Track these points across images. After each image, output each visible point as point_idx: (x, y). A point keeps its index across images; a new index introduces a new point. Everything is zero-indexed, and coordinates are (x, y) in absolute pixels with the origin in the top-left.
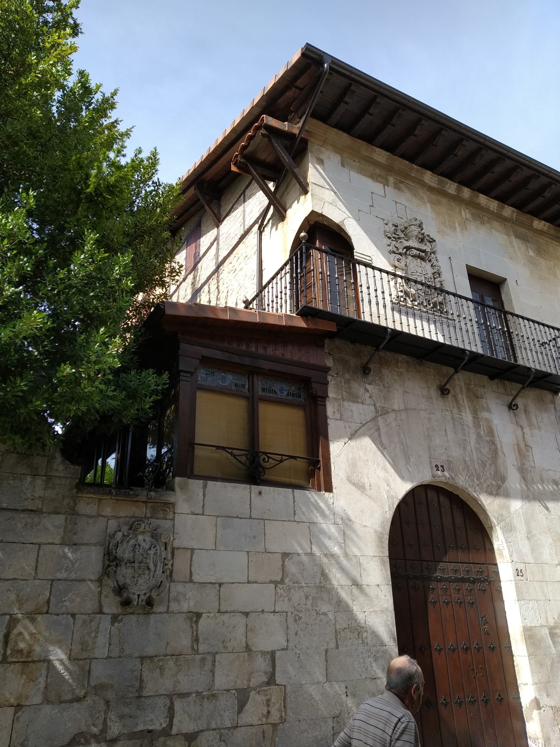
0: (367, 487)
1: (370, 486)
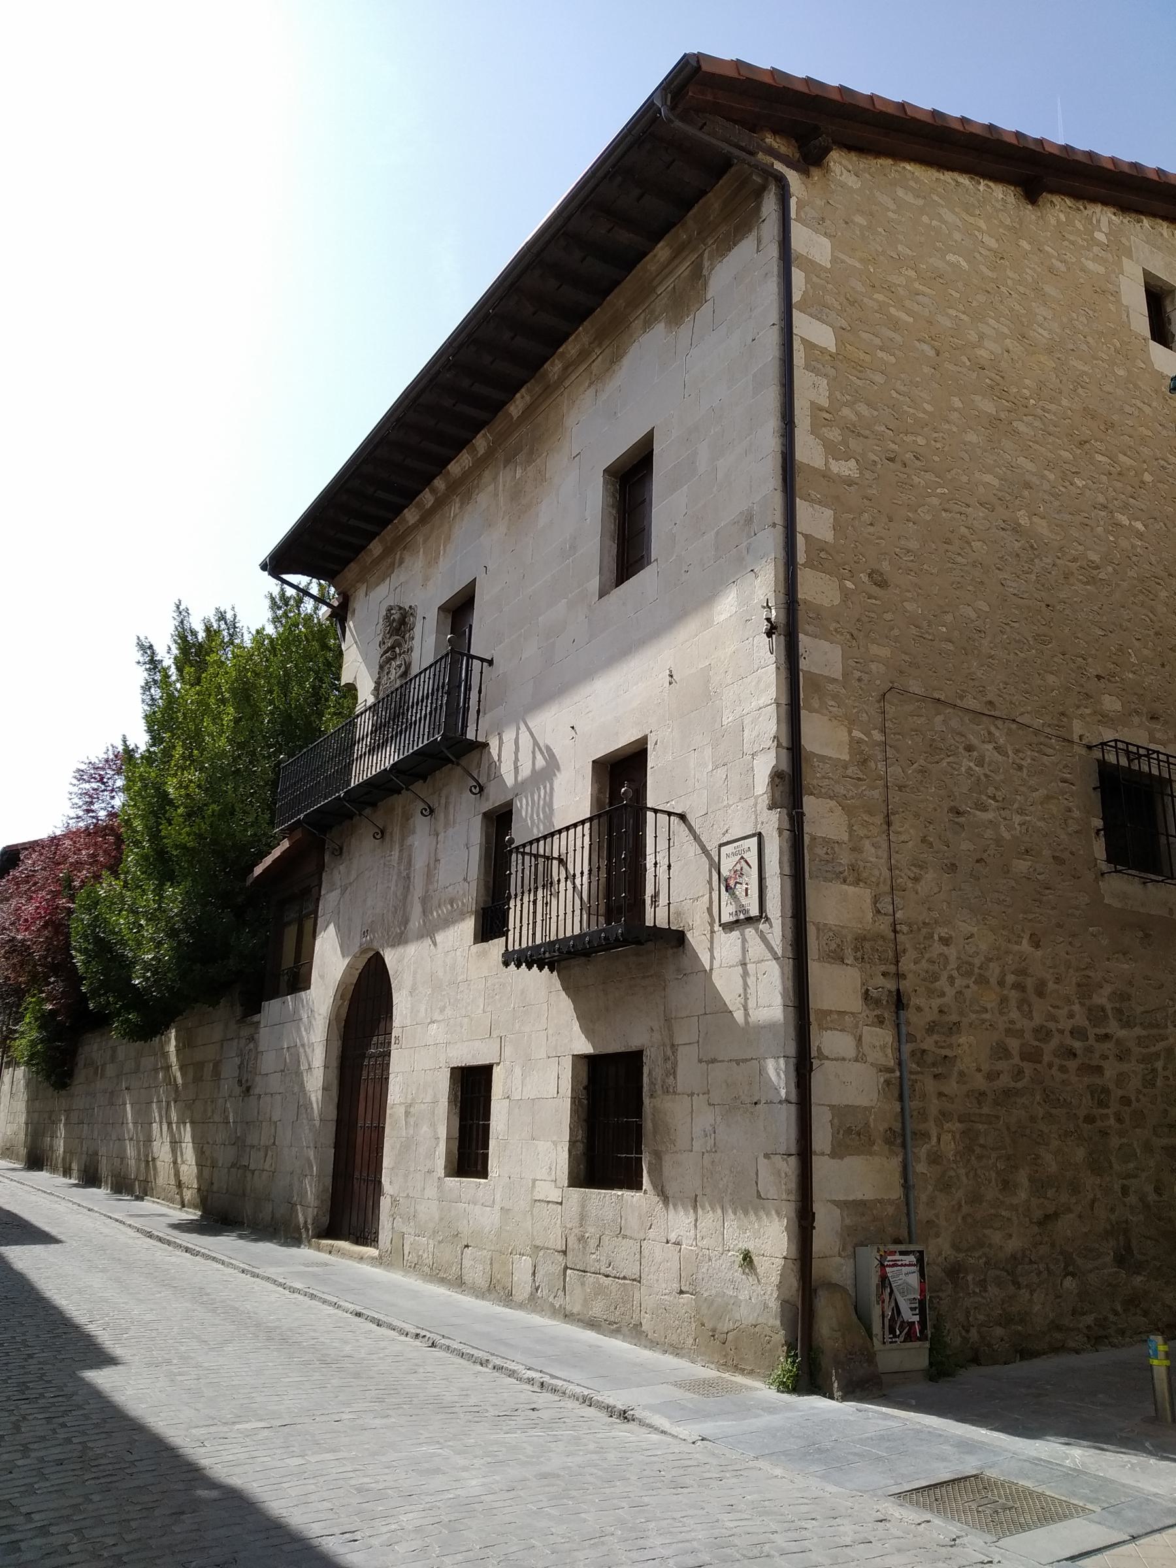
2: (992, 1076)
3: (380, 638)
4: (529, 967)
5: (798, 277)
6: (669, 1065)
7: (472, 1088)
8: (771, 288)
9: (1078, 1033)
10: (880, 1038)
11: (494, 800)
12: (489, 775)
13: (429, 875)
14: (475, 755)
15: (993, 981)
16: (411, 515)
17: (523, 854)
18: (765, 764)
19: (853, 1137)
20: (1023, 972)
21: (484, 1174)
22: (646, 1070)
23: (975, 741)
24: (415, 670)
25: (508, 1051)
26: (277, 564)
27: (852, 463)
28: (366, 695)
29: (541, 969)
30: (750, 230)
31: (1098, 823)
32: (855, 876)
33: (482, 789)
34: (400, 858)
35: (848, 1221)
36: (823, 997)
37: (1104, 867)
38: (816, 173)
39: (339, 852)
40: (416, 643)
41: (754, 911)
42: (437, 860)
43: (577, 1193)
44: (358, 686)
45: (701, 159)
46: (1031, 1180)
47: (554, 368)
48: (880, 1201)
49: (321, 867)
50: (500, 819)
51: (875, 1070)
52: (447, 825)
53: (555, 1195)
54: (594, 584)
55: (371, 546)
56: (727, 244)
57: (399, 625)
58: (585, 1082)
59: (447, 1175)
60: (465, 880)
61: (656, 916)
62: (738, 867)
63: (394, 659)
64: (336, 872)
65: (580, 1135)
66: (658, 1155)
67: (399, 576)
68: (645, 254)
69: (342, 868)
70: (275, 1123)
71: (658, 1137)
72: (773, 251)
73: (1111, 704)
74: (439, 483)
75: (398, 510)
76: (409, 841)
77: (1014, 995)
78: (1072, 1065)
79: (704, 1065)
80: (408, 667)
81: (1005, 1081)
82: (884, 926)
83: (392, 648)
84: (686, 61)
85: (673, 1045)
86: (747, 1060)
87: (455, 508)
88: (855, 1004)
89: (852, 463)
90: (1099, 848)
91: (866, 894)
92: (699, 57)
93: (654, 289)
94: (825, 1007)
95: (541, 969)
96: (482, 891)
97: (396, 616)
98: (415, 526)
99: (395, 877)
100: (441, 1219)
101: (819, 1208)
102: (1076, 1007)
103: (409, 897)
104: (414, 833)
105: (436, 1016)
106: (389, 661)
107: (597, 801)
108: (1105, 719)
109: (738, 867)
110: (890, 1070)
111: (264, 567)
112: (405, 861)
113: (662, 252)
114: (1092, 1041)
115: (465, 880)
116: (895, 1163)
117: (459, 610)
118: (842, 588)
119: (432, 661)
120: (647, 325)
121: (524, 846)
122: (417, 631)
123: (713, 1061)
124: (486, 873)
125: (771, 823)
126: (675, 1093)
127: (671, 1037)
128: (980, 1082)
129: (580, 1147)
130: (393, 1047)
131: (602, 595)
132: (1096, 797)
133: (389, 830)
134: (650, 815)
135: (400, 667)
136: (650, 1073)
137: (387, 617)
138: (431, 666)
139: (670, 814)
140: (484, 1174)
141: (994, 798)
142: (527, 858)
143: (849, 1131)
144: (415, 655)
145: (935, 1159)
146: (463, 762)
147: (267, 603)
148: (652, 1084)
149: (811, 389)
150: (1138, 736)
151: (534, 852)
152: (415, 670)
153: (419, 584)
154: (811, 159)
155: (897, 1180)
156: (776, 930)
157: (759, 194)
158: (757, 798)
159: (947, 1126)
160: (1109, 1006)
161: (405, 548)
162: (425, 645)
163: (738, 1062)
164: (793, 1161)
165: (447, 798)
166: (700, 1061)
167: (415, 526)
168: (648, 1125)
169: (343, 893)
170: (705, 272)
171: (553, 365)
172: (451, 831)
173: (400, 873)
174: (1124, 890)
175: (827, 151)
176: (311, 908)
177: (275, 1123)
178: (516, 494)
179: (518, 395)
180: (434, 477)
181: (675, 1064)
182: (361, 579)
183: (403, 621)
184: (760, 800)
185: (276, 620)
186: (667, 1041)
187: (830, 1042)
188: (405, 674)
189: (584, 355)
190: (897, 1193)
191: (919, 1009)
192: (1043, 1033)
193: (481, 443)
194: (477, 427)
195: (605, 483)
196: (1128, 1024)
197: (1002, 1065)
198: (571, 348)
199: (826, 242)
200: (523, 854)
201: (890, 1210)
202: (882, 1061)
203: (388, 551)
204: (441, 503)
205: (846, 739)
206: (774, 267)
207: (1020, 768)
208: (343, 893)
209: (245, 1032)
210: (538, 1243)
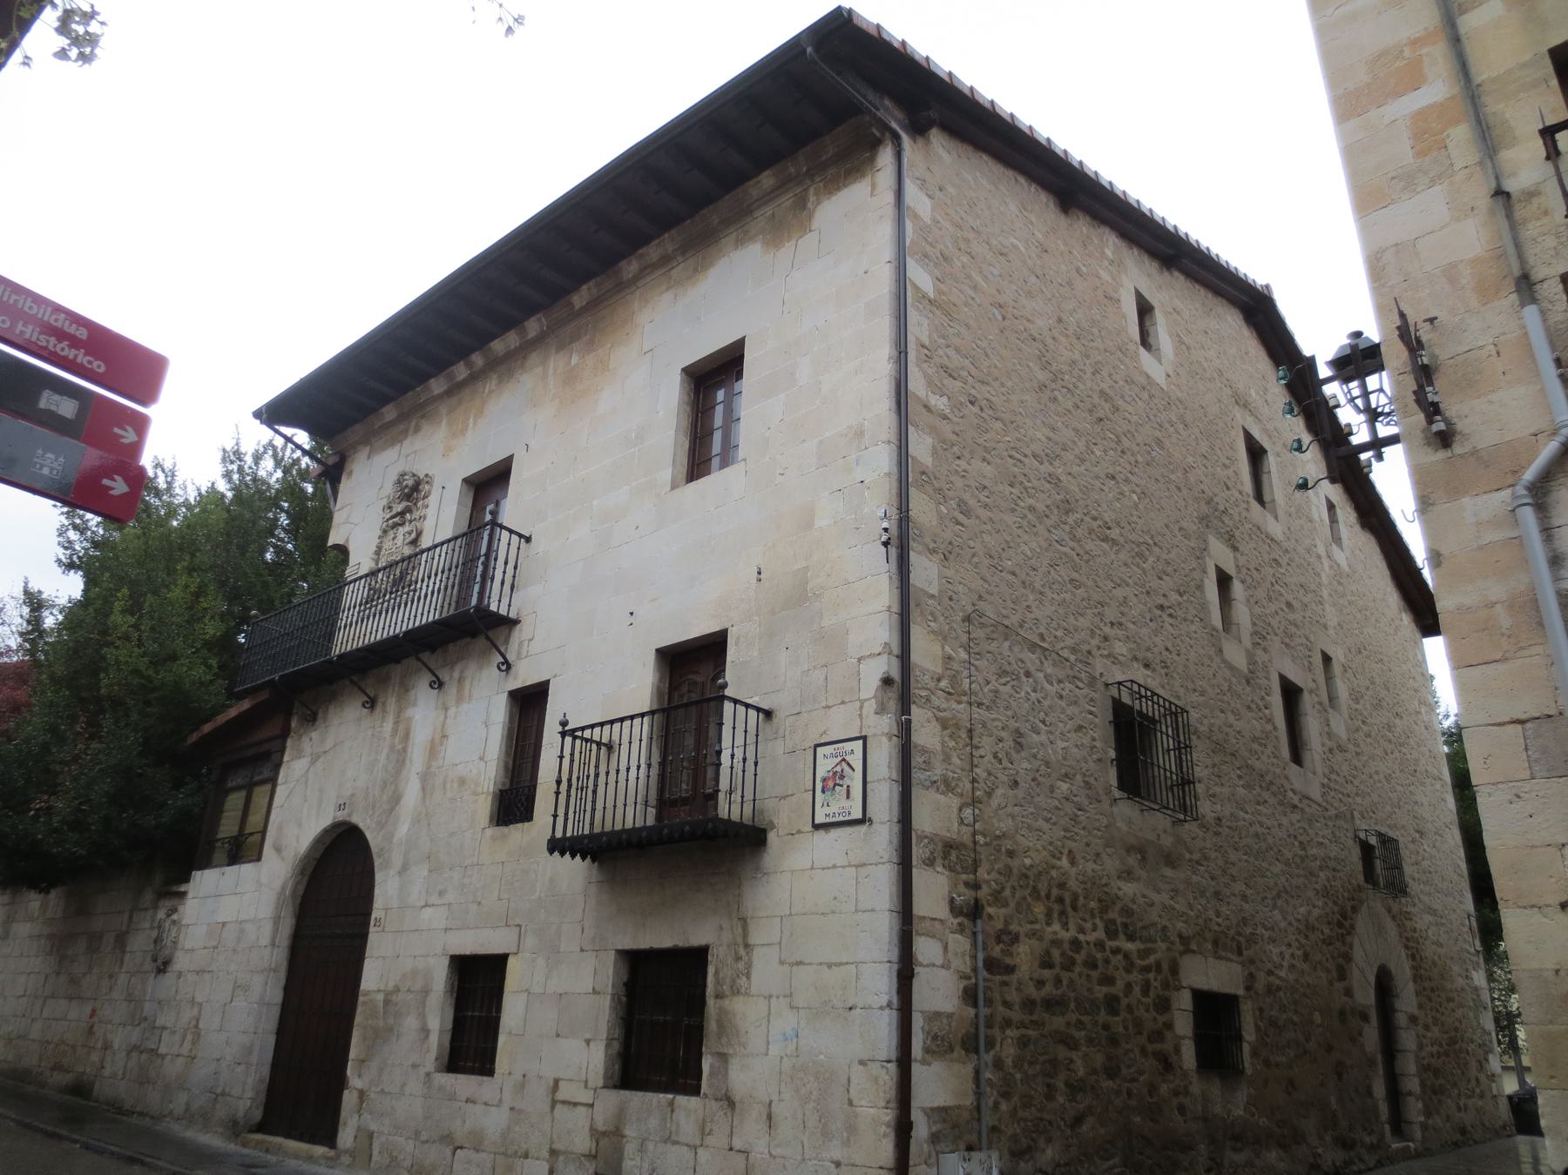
2: (1040, 983)
3: (385, 502)
4: (562, 854)
5: (909, 225)
6: (741, 965)
7: (478, 982)
8: (886, 230)
9: (1100, 945)
10: (960, 943)
11: (524, 676)
12: (519, 653)
13: (433, 750)
14: (504, 630)
15: (1043, 894)
16: (437, 386)
17: (575, 738)
18: (877, 669)
19: (940, 1047)
20: (1062, 886)
21: (490, 1072)
22: (711, 970)
23: (1032, 669)
24: (426, 542)
25: (530, 941)
26: (274, 414)
27: (945, 399)
28: (361, 560)
29: (573, 857)
30: (863, 176)
31: (1112, 754)
32: (947, 786)
33: (509, 667)
34: (395, 732)
35: (934, 1129)
36: (921, 907)
37: (1117, 794)
38: (920, 141)
39: (311, 719)
40: (431, 513)
41: (858, 814)
42: (444, 736)
43: (614, 1097)
44: (351, 549)
45: (830, 108)
46: (1067, 1084)
47: (630, 268)
48: (958, 1107)
49: (285, 734)
50: (529, 703)
51: (956, 977)
52: (460, 699)
53: (585, 1097)
54: (666, 475)
55: (385, 410)
56: (835, 184)
57: (411, 492)
58: (625, 978)
59: (438, 1071)
60: (481, 759)
61: (729, 808)
62: (838, 769)
63: (402, 524)
64: (305, 739)
65: (617, 1033)
66: (723, 1057)
67: (412, 444)
68: (748, 179)
69: (314, 735)
70: (200, 1005)
71: (724, 1040)
72: (889, 197)
73: (1120, 648)
74: (478, 359)
75: (423, 378)
76: (409, 712)
77: (1056, 907)
78: (1095, 974)
79: (786, 968)
80: (419, 534)
81: (1049, 989)
82: (967, 839)
83: (402, 514)
84: (838, 11)
85: (747, 946)
86: (841, 964)
87: (492, 383)
88: (942, 912)
89: (945, 399)
90: (1112, 776)
91: (955, 802)
92: (850, 11)
93: (751, 212)
94: (921, 914)
95: (573, 857)
96: (501, 772)
97: (410, 482)
98: (440, 397)
99: (385, 751)
100: (426, 1118)
101: (917, 1116)
102: (1098, 921)
103: (405, 772)
104: (415, 704)
105: (434, 899)
106: (395, 525)
107: (659, 693)
108: (1114, 658)
109: (838, 769)
110: (968, 978)
111: (257, 415)
112: (401, 733)
113: (767, 180)
114: (1108, 952)
115: (481, 759)
116: (969, 1069)
117: (489, 484)
118: (939, 512)
119: (449, 535)
120: (739, 243)
121: (583, 729)
122: (433, 500)
123: (799, 963)
124: (507, 754)
125: (882, 726)
126: (747, 994)
127: (745, 934)
128: (1031, 991)
129: (616, 1046)
130: (372, 929)
131: (673, 487)
132: (1111, 729)
133: (380, 700)
134: (728, 707)
135: (410, 533)
136: (716, 972)
137: (399, 482)
138: (449, 541)
139: (747, 706)
140: (490, 1072)
141: (1043, 722)
142: (578, 742)
143: (935, 1038)
144: (428, 526)
145: (998, 1064)
146: (490, 634)
147: (220, 454)
148: (718, 982)
149: (920, 327)
150: (1140, 674)
151: (596, 738)
152: (426, 542)
153: (444, 454)
154: (919, 130)
155: (970, 1086)
156: (883, 836)
157: (875, 145)
158: (862, 702)
159: (1008, 1032)
160: (1119, 921)
161: (423, 416)
162: (442, 516)
163: (830, 966)
164: (892, 1067)
165: (462, 672)
166: (782, 963)
167: (440, 397)
168: (711, 1026)
169: (313, 762)
170: (810, 205)
171: (629, 263)
172: (465, 706)
173: (392, 747)
174: (1126, 812)
175: (929, 127)
176: (266, 774)
177: (200, 1005)
178: (570, 378)
179: (585, 287)
180: (472, 351)
181: (749, 965)
182: (366, 440)
183: (416, 488)
184: (866, 704)
185: (227, 475)
186: (740, 940)
187: (926, 949)
188: (414, 542)
189: (665, 260)
190: (969, 1101)
191: (990, 917)
192: (1076, 944)
193: (533, 326)
194: (532, 310)
195: (682, 381)
196: (1131, 938)
197: (1047, 973)
198: (653, 252)
199: (927, 201)
200: (575, 738)
201: (966, 1115)
202: (962, 968)
203: (404, 417)
204: (475, 378)
205: (940, 653)
206: (889, 211)
207: (1061, 697)
208: (313, 762)
209: (167, 903)
210: (557, 1146)
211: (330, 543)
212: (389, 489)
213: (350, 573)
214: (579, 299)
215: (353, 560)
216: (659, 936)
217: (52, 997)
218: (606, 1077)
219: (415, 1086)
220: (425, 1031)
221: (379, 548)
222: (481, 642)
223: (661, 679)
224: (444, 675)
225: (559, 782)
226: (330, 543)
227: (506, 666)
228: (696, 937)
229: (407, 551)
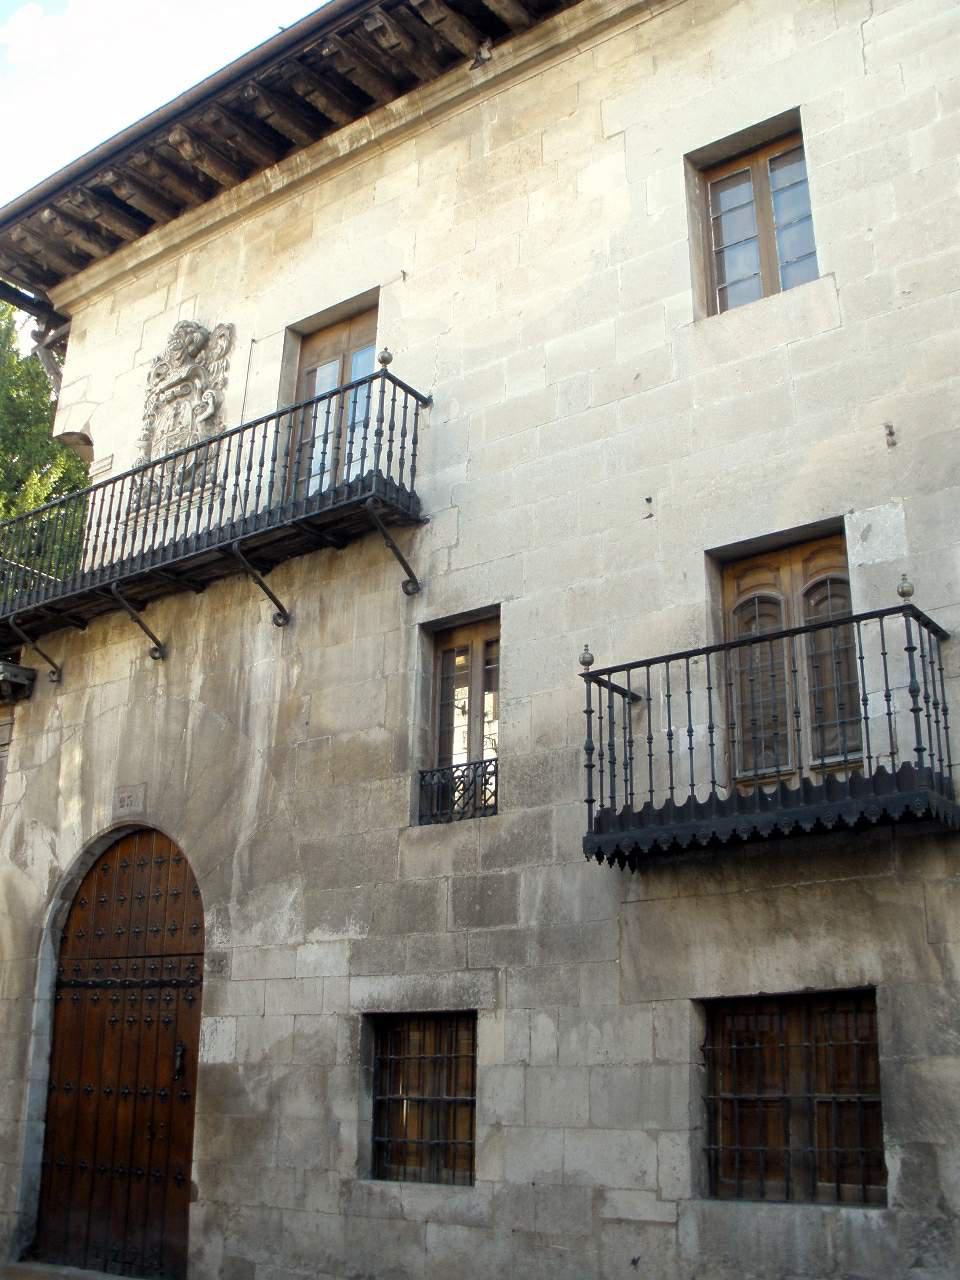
0: (29, 862)
1: (33, 859)
119: (274, 410)
144: (231, 396)
188: (210, 420)
211: (57, 431)
212: (159, 342)
213: (97, 472)
214: (341, 140)
215: (99, 451)
216: (775, 968)
217: (450, 548)
218: (696, 1185)
219: (323, 1201)
220: (329, 1126)
221: (151, 431)
222: (375, 548)
223: (714, 600)
224: (301, 606)
225: (589, 712)
226: (57, 431)
227: (412, 587)
228: (860, 960)
229: (201, 433)
